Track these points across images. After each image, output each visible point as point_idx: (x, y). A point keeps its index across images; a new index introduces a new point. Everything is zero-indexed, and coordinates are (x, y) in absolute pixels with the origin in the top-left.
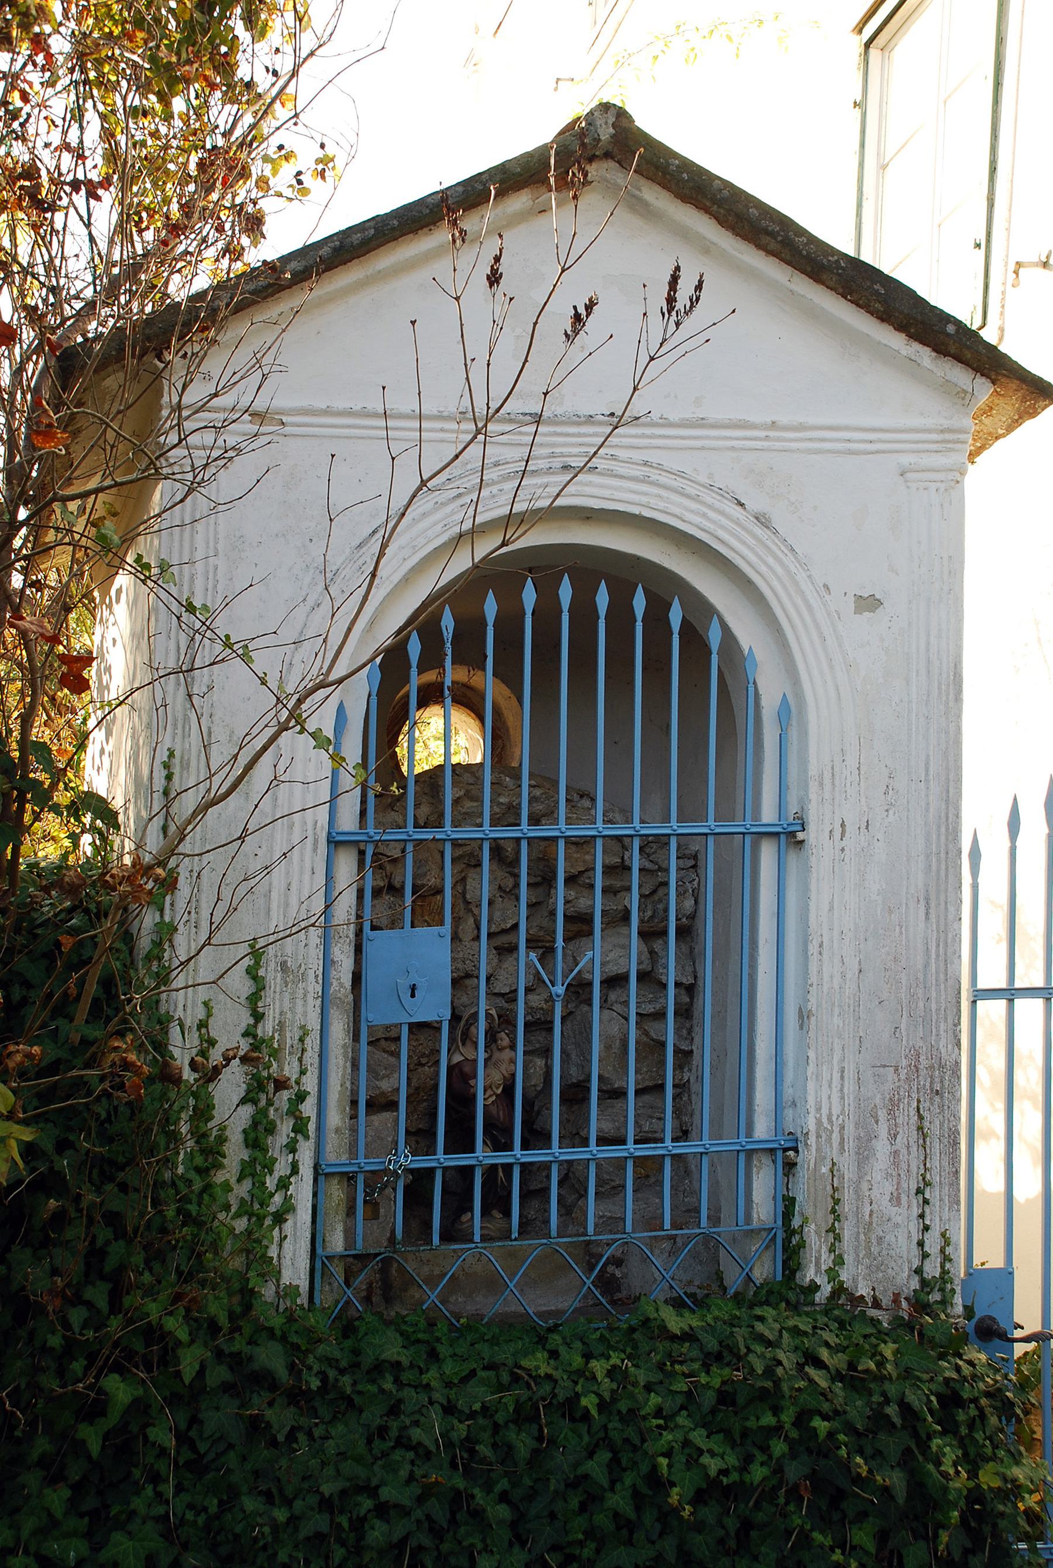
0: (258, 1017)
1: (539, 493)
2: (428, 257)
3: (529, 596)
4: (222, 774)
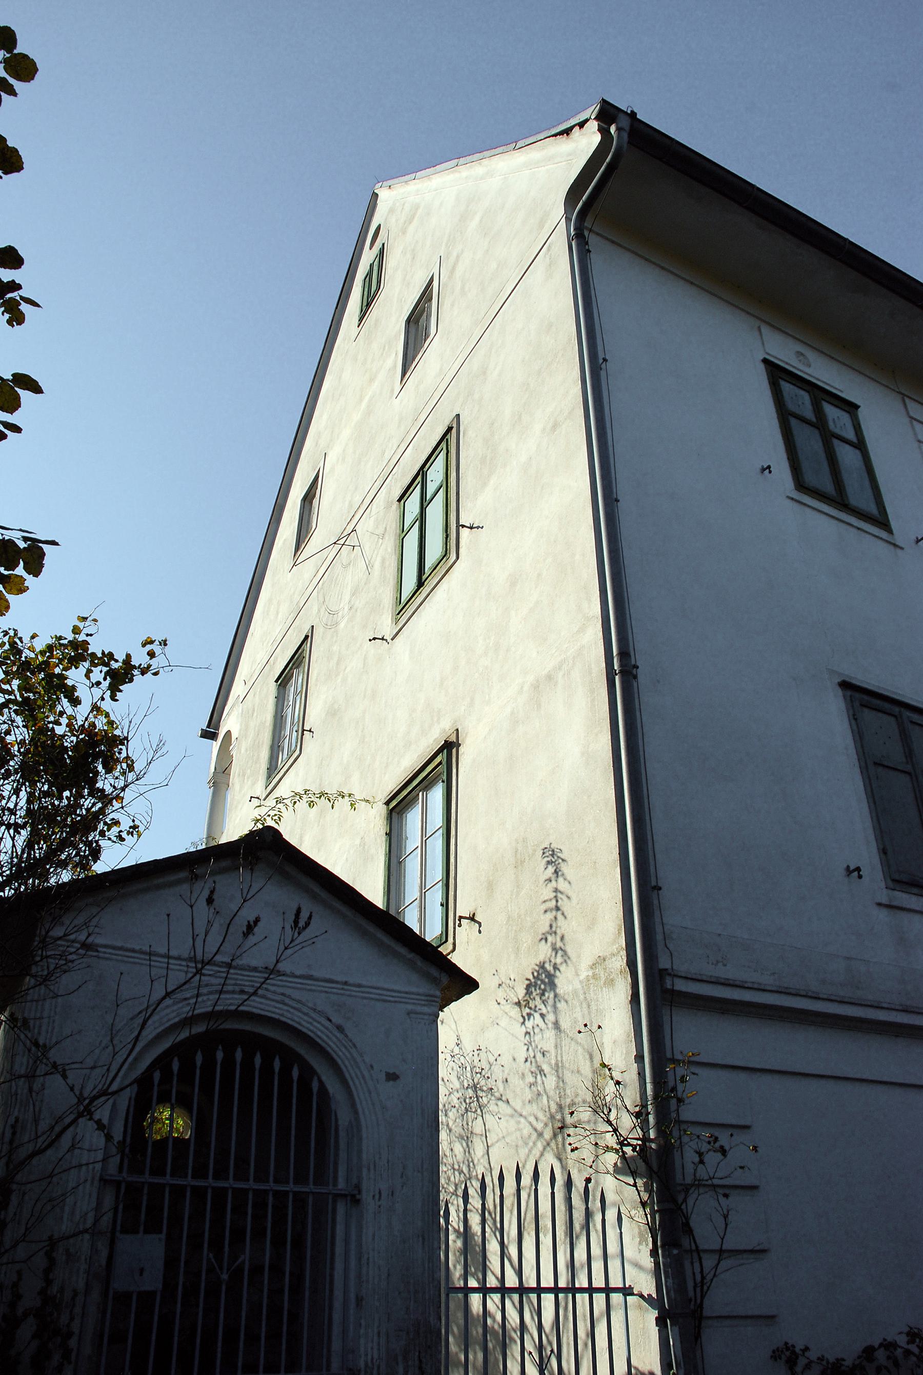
0: (49, 1282)
1: (230, 1002)
2: (179, 882)
3: (220, 1055)
4: (45, 1136)
